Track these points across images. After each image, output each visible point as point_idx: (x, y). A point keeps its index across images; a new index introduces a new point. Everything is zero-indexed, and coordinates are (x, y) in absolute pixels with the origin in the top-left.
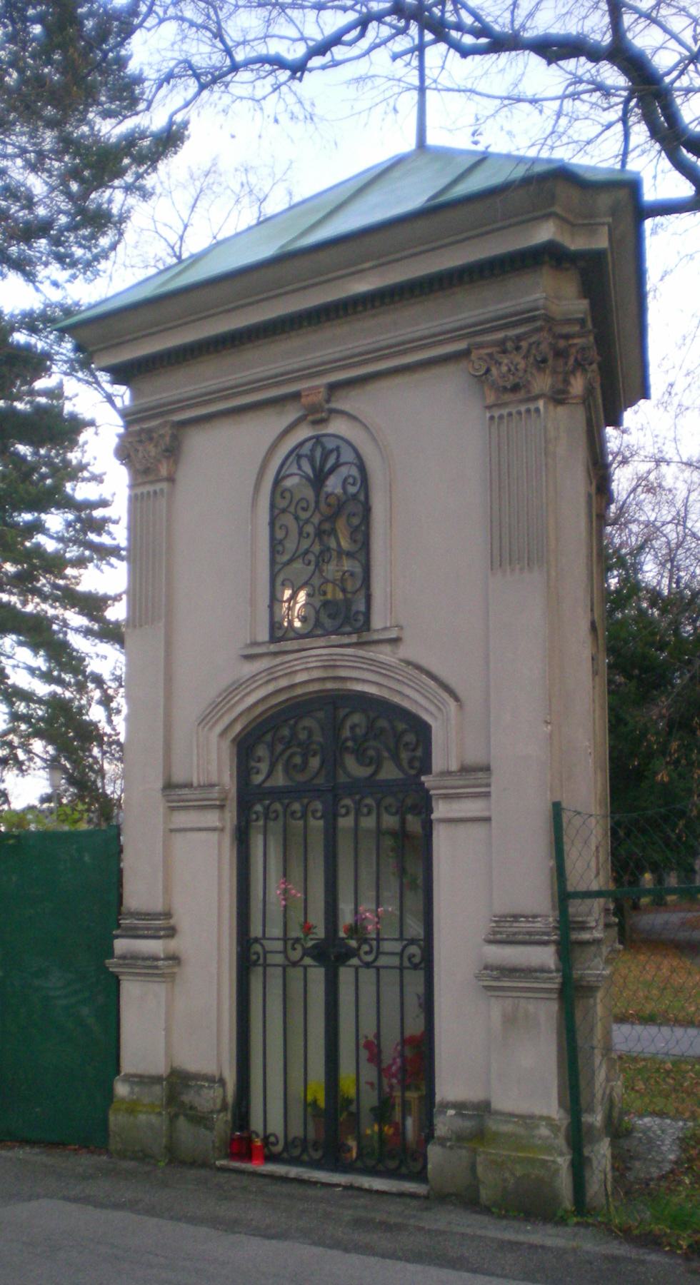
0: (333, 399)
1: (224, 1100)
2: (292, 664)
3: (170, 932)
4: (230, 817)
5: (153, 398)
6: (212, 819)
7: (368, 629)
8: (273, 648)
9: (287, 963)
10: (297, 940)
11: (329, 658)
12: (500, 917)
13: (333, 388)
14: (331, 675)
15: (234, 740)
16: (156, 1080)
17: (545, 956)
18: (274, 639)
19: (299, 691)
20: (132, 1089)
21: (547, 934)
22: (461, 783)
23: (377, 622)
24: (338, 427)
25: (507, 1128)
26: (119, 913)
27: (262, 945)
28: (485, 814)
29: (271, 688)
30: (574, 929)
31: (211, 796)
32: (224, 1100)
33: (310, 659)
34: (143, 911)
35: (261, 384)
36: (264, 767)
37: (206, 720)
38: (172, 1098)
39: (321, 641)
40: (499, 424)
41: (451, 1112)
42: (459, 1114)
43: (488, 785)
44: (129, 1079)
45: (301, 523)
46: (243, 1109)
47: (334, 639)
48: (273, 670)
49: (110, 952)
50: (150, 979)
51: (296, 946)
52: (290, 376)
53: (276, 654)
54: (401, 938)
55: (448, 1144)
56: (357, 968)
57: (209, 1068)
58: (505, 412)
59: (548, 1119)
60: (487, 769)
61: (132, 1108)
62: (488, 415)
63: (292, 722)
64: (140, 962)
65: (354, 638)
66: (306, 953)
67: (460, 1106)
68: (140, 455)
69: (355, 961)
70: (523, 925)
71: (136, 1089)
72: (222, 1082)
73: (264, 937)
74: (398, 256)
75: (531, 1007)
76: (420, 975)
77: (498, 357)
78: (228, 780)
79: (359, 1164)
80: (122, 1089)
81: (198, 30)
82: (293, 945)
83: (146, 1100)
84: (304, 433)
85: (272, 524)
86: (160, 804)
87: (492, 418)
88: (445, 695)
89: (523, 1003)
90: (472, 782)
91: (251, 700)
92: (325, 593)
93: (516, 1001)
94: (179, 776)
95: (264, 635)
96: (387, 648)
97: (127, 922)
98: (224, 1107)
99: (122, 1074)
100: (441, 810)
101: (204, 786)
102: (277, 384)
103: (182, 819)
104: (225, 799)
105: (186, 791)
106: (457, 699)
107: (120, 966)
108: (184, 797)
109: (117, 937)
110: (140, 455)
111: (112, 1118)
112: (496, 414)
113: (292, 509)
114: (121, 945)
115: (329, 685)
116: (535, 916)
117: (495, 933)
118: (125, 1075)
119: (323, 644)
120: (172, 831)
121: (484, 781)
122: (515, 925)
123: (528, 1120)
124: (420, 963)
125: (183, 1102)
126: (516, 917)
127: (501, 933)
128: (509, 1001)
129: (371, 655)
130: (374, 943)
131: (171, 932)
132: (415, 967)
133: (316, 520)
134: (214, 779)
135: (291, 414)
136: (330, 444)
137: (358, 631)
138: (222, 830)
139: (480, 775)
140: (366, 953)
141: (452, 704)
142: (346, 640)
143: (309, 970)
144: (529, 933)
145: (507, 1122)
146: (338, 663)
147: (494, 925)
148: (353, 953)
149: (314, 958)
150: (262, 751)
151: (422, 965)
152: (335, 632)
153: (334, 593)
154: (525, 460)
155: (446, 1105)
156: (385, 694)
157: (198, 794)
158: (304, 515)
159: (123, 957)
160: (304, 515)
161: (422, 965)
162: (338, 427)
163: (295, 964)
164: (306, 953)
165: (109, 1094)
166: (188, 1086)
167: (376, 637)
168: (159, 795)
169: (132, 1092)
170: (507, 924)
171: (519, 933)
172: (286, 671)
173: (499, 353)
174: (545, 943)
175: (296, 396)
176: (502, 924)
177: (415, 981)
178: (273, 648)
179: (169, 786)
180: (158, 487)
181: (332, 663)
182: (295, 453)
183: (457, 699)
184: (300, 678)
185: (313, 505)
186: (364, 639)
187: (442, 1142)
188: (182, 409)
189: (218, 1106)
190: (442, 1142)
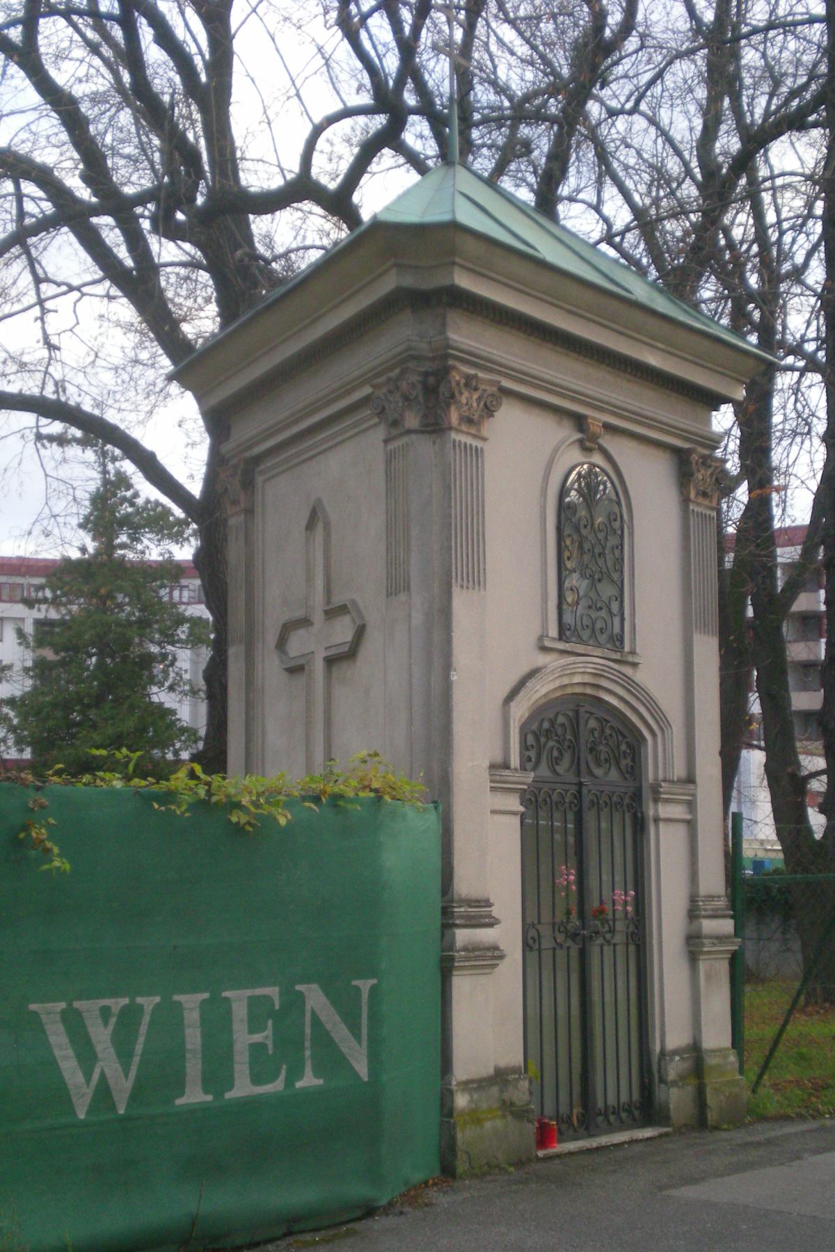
5: (467, 341)
13: (608, 427)
20: (472, 1097)
34: (473, 898)
35: (526, 378)
41: (677, 1058)
44: (466, 1085)
50: (481, 971)
52: (507, 371)
61: (475, 1117)
71: (475, 1096)
74: (606, 322)
83: (484, 1106)
95: (553, 631)
97: (462, 909)
102: (573, 399)
111: (459, 1135)
119: (600, 655)
121: (691, 792)
130: (611, 923)
159: (465, 949)
169: (471, 1101)
187: (674, 1083)
190: (674, 1083)
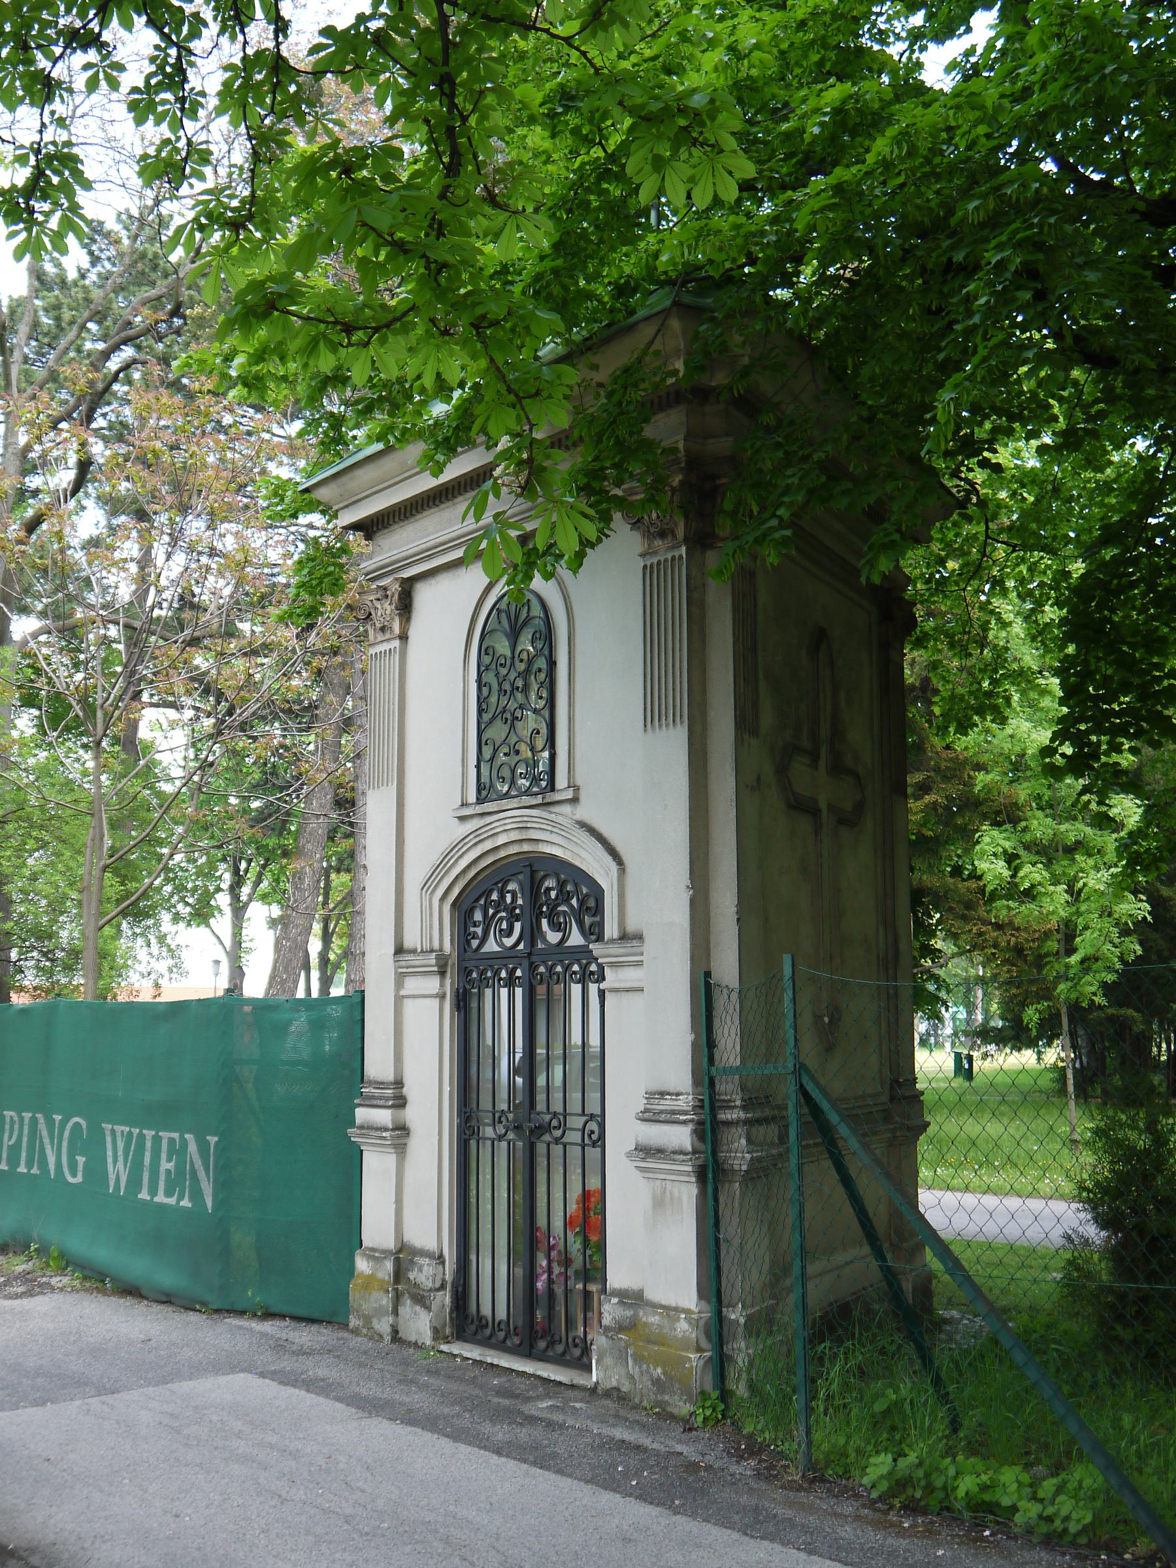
1: (444, 1280)
7: (553, 789)
8: (479, 809)
16: (386, 1253)
18: (480, 801)
19: (502, 853)
21: (685, 1113)
26: (362, 1081)
30: (721, 1107)
32: (444, 1280)
37: (427, 886)
39: (514, 803)
42: (621, 1303)
47: (527, 800)
49: (352, 1122)
54: (583, 1114)
57: (431, 1244)
59: (687, 1312)
65: (539, 800)
72: (440, 1259)
80: (362, 1265)
81: (651, 270)
90: (629, 950)
91: (463, 863)
95: (472, 797)
98: (443, 1287)
107: (360, 1135)
109: (360, 1105)
115: (526, 847)
116: (678, 1094)
117: (646, 1111)
123: (671, 1312)
126: (662, 1094)
129: (552, 817)
131: (400, 1102)
132: (594, 1145)
133: (513, 675)
137: (542, 792)
139: (635, 943)
144: (673, 1112)
154: (266, 571)
159: (362, 1127)
160: (504, 671)
165: (351, 1270)
174: (684, 1122)
177: (593, 1153)
178: (479, 809)
179: (399, 950)
184: (501, 840)
186: (548, 800)
188: (410, 565)
189: (438, 1285)
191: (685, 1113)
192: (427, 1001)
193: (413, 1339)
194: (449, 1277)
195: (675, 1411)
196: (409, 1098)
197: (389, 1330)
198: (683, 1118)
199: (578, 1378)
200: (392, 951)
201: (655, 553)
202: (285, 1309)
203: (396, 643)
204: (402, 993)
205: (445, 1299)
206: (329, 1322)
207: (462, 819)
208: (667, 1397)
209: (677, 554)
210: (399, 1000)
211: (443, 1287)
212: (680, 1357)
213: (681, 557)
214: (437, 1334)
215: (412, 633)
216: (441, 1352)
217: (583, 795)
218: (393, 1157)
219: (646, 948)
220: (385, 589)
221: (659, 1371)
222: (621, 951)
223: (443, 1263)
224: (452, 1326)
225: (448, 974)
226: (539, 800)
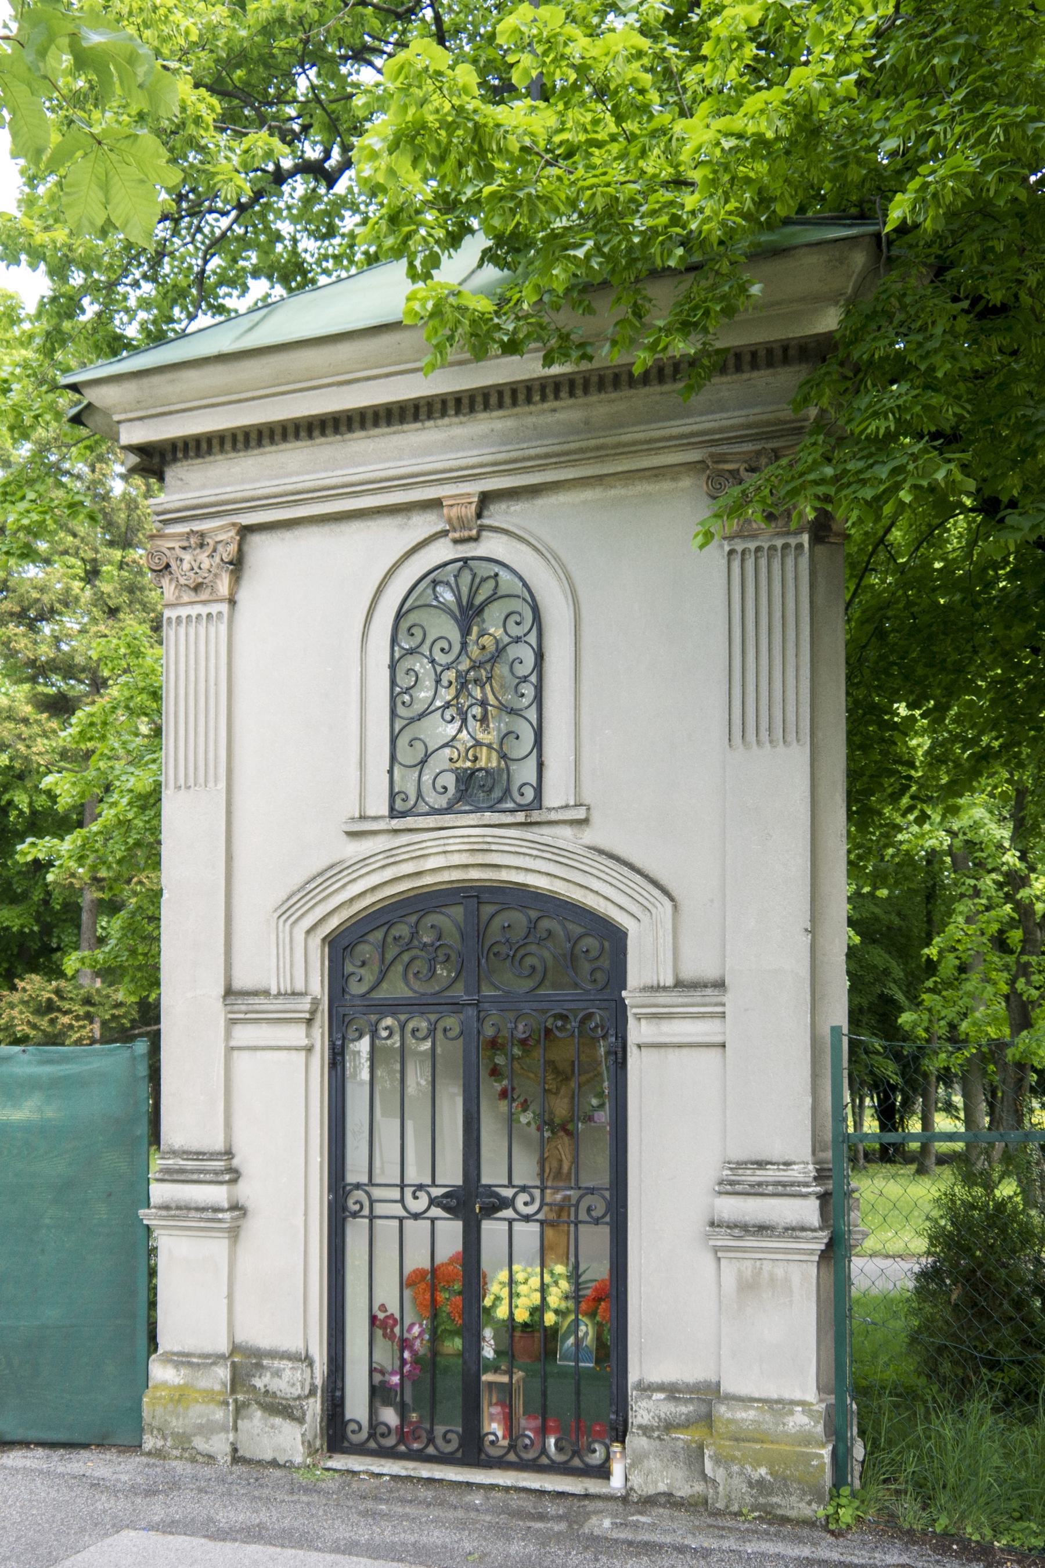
0: (486, 513)
2: (424, 845)
3: (234, 1176)
4: (320, 1035)
6: (297, 1035)
8: (396, 824)
9: (405, 1214)
10: (420, 1187)
11: (480, 840)
12: (737, 1163)
14: (480, 862)
15: (324, 940)
16: (218, 1358)
17: (808, 1211)
19: (428, 880)
22: (680, 1000)
23: (556, 794)
24: (492, 546)
25: (746, 1415)
27: (368, 1193)
28: (718, 1039)
29: (388, 874)
31: (300, 1007)
33: (451, 841)
36: (369, 976)
38: (238, 1380)
40: (783, 557)
43: (724, 1005)
44: (181, 1360)
45: (439, 669)
46: (338, 1394)
47: (489, 817)
48: (394, 852)
51: (418, 1194)
53: (396, 831)
55: (656, 1434)
56: (510, 1221)
57: (293, 1343)
58: (752, 545)
60: (720, 985)
61: (180, 1396)
62: (727, 548)
63: (413, 919)
64: (193, 1214)
65: (520, 817)
66: (433, 1202)
67: (672, 1391)
68: (186, 566)
69: (508, 1213)
70: (770, 1174)
72: (309, 1361)
73: (371, 1183)
75: (780, 1271)
76: (604, 1232)
77: (743, 474)
78: (318, 986)
79: (512, 1457)
80: (161, 1373)
82: (414, 1193)
84: (443, 552)
85: (393, 667)
86: (218, 1011)
87: (731, 552)
88: (657, 893)
89: (767, 1266)
90: (698, 1000)
92: (476, 759)
93: (758, 1263)
94: (240, 982)
95: (379, 806)
96: (567, 832)
98: (312, 1393)
99: (160, 1351)
100: (637, 1032)
101: (286, 994)
103: (244, 1035)
104: (313, 1012)
105: (261, 1000)
106: (672, 899)
108: (257, 1007)
110: (186, 566)
112: (739, 548)
113: (425, 649)
114: (159, 1192)
115: (474, 874)
116: (787, 1164)
118: (165, 1353)
119: (472, 823)
120: (233, 1048)
122: (758, 1172)
123: (780, 1406)
124: (603, 1216)
125: (255, 1386)
126: (761, 1164)
127: (738, 1183)
128: (749, 1263)
131: (234, 1176)
134: (300, 986)
135: (424, 525)
136: (485, 570)
138: (309, 1049)
140: (526, 1204)
141: (668, 904)
142: (508, 819)
143: (438, 1223)
145: (746, 1409)
146: (493, 847)
147: (729, 1172)
148: (508, 1203)
149: (447, 1209)
150: (365, 950)
151: (607, 1219)
152: (491, 809)
153: (489, 759)
155: (647, 1389)
156: (560, 888)
157: (279, 1004)
158: (441, 659)
161: (607, 1219)
162: (492, 546)
163: (416, 1216)
164: (433, 1202)
166: (259, 1366)
167: (553, 816)
168: (219, 1004)
170: (749, 1172)
171: (767, 1184)
172: (414, 855)
173: (747, 470)
175: (436, 504)
176: (740, 1172)
179: (229, 992)
180: (214, 608)
181: (485, 847)
182: (432, 578)
183: (672, 899)
184: (431, 863)
185: (457, 648)
191: (806, 1185)
192: (294, 1054)
193: (268, 1456)
194: (319, 1382)
195: (792, 1514)
196: (243, 1170)
197: (228, 1449)
198: (804, 1190)
199: (593, 1486)
200: (222, 992)
201: (753, 537)
202: (32, 1435)
203: (224, 607)
204: (233, 1043)
205: (315, 1407)
206: (98, 1445)
207: (352, 835)
208: (775, 1500)
209: (793, 541)
210: (230, 1050)
211: (312, 1393)
212: (803, 1454)
213: (800, 546)
214: (312, 1451)
215: (242, 596)
216: (328, 1469)
217: (596, 817)
218: (224, 1244)
219: (728, 998)
220: (202, 535)
221: (763, 1471)
222: (680, 1000)
223: (311, 1365)
224: (322, 1438)
225: (317, 1023)
226: (520, 817)
